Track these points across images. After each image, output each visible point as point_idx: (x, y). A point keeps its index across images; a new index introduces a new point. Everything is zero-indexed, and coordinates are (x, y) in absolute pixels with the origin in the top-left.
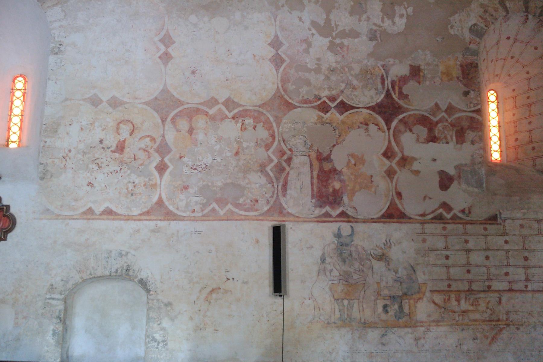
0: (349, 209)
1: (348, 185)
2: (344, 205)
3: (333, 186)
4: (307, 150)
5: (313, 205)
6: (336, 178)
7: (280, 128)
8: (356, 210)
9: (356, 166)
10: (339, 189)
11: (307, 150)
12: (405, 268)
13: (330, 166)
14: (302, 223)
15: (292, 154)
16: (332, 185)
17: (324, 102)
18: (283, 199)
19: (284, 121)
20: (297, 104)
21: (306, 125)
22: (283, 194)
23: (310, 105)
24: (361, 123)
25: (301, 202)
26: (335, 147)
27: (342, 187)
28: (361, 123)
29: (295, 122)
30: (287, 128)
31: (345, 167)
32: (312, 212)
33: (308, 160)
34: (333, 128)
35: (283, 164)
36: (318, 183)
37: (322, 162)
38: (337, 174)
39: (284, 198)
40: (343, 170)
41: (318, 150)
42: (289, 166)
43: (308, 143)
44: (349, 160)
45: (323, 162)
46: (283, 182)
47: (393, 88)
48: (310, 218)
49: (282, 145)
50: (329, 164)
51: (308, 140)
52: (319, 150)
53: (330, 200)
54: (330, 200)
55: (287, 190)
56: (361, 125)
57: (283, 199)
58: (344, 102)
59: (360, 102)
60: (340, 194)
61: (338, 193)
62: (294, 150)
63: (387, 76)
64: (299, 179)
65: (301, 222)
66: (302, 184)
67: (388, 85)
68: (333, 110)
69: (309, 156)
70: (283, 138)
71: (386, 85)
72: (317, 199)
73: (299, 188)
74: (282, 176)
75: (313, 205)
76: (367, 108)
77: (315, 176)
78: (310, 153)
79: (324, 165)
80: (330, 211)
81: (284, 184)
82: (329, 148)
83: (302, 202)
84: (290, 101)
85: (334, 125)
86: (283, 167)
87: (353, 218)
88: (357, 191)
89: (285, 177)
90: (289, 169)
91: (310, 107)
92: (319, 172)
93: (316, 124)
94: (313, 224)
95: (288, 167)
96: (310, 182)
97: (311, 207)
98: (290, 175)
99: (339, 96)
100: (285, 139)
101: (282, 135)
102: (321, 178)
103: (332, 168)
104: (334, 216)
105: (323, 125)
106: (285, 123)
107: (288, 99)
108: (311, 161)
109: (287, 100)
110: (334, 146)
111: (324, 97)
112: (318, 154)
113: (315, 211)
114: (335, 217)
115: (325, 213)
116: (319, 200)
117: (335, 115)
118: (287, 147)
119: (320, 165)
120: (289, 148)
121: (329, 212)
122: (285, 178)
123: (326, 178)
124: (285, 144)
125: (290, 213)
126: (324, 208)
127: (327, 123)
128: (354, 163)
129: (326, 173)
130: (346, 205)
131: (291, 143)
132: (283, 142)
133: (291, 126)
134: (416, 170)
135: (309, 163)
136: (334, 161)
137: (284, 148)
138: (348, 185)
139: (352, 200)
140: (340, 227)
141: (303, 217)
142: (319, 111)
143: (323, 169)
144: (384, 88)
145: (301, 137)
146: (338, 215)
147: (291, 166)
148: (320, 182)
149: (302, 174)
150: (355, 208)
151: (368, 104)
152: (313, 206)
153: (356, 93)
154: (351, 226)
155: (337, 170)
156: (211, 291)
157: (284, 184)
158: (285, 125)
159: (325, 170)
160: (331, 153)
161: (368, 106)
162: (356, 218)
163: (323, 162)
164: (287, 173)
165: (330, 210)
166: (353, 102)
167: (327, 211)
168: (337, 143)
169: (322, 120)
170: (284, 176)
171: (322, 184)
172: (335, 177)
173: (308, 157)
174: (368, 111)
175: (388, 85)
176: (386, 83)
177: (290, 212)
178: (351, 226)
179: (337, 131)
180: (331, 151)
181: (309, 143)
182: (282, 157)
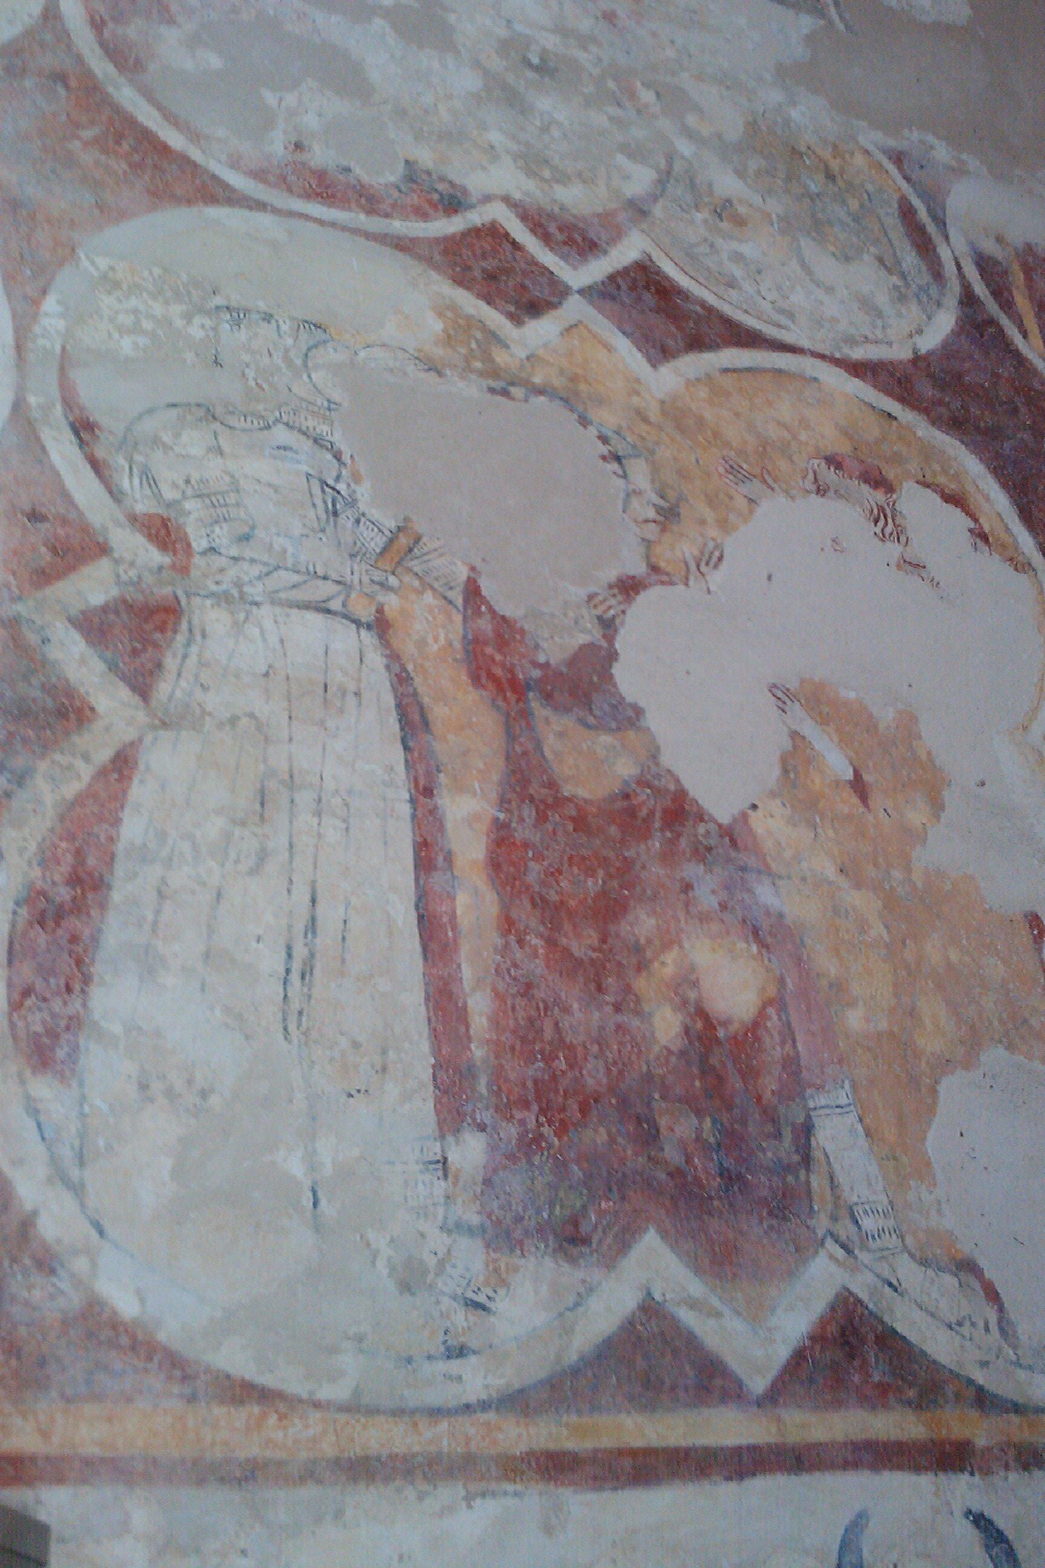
0: (908, 1272)
1: (839, 986)
2: (846, 1229)
3: (688, 978)
4: (360, 568)
5: (475, 1219)
6: (707, 896)
7: (50, 304)
8: (992, 1295)
9: (877, 800)
10: (756, 1025)
11: (358, 573)
12: (713, 892)
13: (625, 769)
14: (308, 1492)
15: (184, 570)
16: (668, 965)
17: (494, 233)
18: (33, 1110)
19: (103, 263)
20: (236, 180)
21: (330, 355)
22: (36, 1021)
23: (362, 217)
24: (834, 462)
25: (295, 1167)
26: (644, 598)
27: (778, 1002)
28: (834, 462)
29: (218, 301)
30: (122, 330)
31: (773, 794)
32: (460, 1318)
33: (376, 659)
34: (604, 439)
35: (54, 653)
36: (508, 924)
37: (526, 714)
38: (702, 853)
39: (43, 1088)
40: (758, 823)
41: (472, 591)
42: (143, 689)
43: (362, 506)
44: (794, 735)
45: (535, 703)
46: (47, 859)
47: (1001, 293)
48: (436, 1413)
49: (55, 457)
50: (605, 739)
51: (357, 478)
52: (487, 587)
53: (672, 1154)
54: (672, 1154)
55: (99, 969)
56: (830, 476)
57: (33, 1110)
58: (667, 278)
59: (791, 315)
60: (769, 1084)
61: (749, 1074)
62: (199, 544)
63: (941, 223)
64: (263, 855)
65: (309, 1474)
66: (312, 926)
67: (959, 267)
68: (574, 308)
69: (381, 625)
70: (69, 402)
71: (950, 269)
72: (510, 1131)
73: (271, 962)
74: (40, 783)
75: (475, 1219)
76: (858, 369)
77: (431, 1008)
78: (392, 603)
79: (551, 744)
80: (693, 1304)
81: (64, 894)
82: (583, 593)
83: (313, 1166)
84: (175, 140)
85: (608, 418)
86: (48, 689)
87: (983, 1400)
88: (945, 1065)
89: (80, 800)
90: (141, 716)
91: (368, 236)
92: (503, 802)
93: (434, 368)
94: (488, 1509)
95: (124, 693)
96: (405, 916)
97: (438, 1241)
98: (139, 791)
99: (617, 234)
100: (96, 416)
101: (62, 371)
102: (534, 872)
103: (642, 782)
104: (758, 1385)
105: (505, 393)
106: (109, 283)
107: (148, 117)
108: (401, 679)
109: (131, 122)
110: (629, 587)
111: (487, 199)
112: (485, 625)
113: (501, 1304)
114: (773, 1396)
115: (629, 1325)
116: (531, 1143)
117: (609, 348)
118: (115, 494)
119: (511, 737)
120: (143, 506)
121: (687, 1317)
122: (69, 810)
123: (593, 885)
124: (95, 465)
125: (116, 1324)
126: (610, 1263)
127: (540, 391)
128: (849, 775)
129: (580, 822)
130: (868, 1223)
131: (169, 476)
132: (69, 435)
133: (179, 323)
134: (67, 487)
135: (389, 700)
136: (653, 721)
137: (79, 498)
138: (839, 986)
139: (924, 1170)
140: (857, 1525)
141: (325, 1393)
142: (460, 281)
143: (552, 785)
144: (938, 275)
145: (282, 435)
146: (799, 1356)
147: (163, 689)
148: (524, 913)
149: (305, 798)
150: (967, 1267)
151: (851, 341)
152: (457, 1228)
153: (747, 249)
154: (980, 1521)
155: (701, 816)
156: (682, 432)
157: (64, 894)
158: (107, 301)
159: (567, 790)
160: (610, 639)
161: (858, 354)
162: (1017, 1408)
163: (535, 703)
164: (103, 755)
165: (696, 1287)
166: (733, 294)
167: (650, 1308)
168: (655, 569)
169: (488, 358)
170: (71, 789)
171: (551, 943)
172: (687, 887)
173: (368, 638)
174: (855, 386)
175: (959, 267)
176: (944, 253)
177: (127, 1306)
178: (980, 1521)
179: (640, 473)
180: (609, 626)
181: (375, 514)
182: (44, 577)
